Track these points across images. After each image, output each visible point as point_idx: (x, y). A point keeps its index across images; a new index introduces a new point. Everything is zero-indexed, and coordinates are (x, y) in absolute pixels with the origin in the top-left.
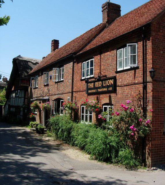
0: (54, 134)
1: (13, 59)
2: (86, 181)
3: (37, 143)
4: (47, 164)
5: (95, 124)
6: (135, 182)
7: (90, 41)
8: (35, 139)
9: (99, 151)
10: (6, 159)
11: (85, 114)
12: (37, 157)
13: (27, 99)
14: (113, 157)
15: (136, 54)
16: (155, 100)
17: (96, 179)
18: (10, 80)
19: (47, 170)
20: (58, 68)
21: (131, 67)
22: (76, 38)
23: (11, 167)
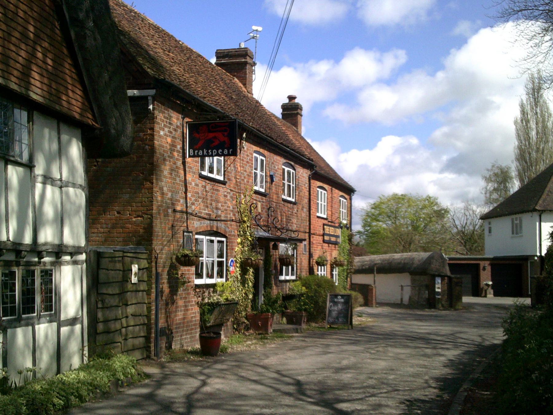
0: (495, 194)
1: (282, 106)
2: (160, 377)
3: (368, 239)
4: (522, 99)
5: (437, 199)
6: (326, 392)
7: (395, 331)
8: (466, 357)
9: (295, 242)
10: (461, 333)
11: (286, 182)
12: (196, 380)
13: (179, 208)
14: (165, 115)
15: (491, 299)
16: (516, 220)
17: (373, 380)
18: (545, 255)
19: (59, 295)
20: (223, 157)
21: (165, 79)
22: (171, 33)
23: (245, 410)
